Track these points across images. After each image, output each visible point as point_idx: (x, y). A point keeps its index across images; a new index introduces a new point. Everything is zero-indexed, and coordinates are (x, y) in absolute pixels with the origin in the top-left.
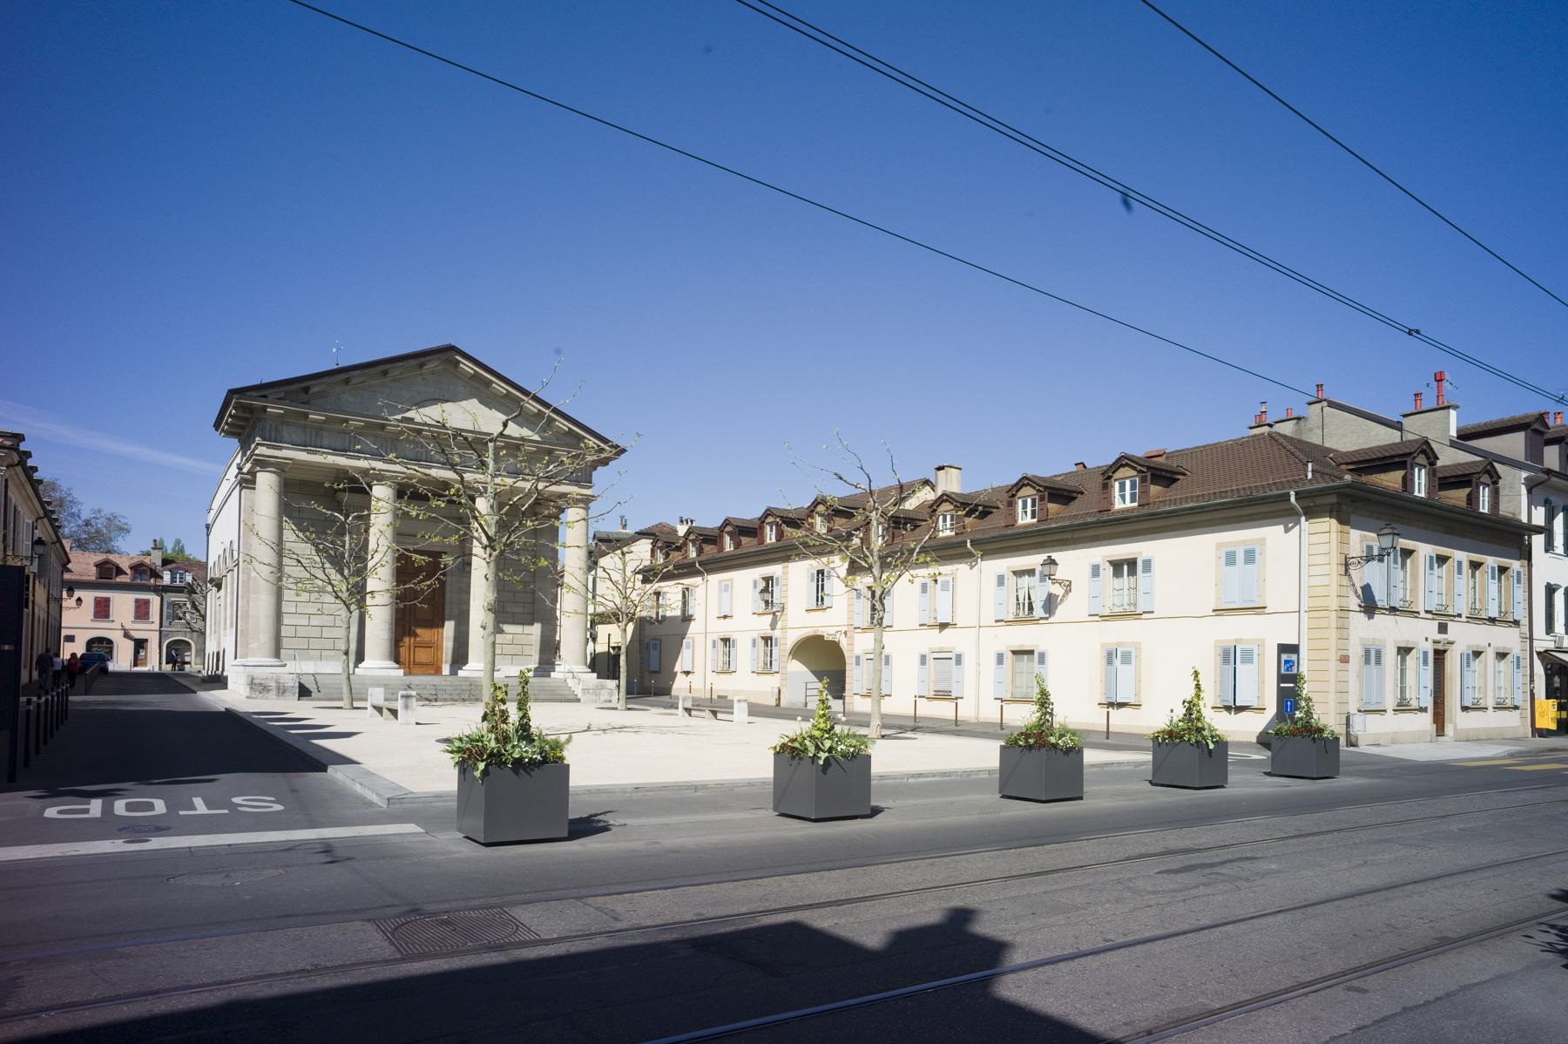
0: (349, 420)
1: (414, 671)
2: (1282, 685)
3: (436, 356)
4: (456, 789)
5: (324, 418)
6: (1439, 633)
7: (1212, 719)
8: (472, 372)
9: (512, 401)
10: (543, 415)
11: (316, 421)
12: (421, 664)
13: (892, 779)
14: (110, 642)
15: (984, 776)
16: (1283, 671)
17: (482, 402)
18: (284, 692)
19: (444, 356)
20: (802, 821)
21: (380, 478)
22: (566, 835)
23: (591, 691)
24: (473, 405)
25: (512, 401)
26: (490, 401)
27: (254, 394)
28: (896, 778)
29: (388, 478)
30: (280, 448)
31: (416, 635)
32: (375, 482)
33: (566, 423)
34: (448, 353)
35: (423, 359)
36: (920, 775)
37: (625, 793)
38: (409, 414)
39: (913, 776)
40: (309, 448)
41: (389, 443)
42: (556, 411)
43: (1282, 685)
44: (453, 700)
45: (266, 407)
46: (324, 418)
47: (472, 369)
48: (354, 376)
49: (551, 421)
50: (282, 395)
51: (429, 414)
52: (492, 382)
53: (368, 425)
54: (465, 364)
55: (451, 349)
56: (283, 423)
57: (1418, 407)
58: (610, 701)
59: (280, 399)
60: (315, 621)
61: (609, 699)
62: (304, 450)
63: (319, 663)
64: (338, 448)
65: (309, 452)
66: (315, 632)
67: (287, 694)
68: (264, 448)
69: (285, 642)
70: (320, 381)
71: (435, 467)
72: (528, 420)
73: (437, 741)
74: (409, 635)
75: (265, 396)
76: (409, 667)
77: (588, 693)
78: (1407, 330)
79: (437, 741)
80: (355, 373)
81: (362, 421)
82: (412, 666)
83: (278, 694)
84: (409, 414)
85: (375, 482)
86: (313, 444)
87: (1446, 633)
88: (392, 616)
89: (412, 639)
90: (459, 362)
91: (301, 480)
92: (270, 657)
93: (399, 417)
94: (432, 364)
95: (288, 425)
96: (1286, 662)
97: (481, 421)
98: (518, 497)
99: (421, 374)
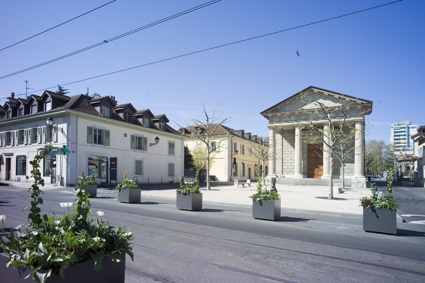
0: (285, 113)
2: (116, 169)
3: (307, 90)
4: (176, 197)
5: (361, 107)
7: (268, 187)
11: (279, 115)
13: (213, 203)
15: (250, 207)
17: (323, 99)
18: (269, 181)
19: (309, 90)
20: (106, 199)
21: (357, 122)
22: (128, 202)
23: (355, 183)
25: (331, 96)
27: (265, 112)
28: (214, 203)
30: (273, 124)
31: (319, 168)
32: (356, 123)
33: (349, 98)
36: (223, 203)
37: (149, 197)
38: (303, 108)
39: (221, 203)
40: (279, 122)
41: (298, 117)
42: (345, 96)
43: (116, 169)
45: (276, 114)
46: (361, 107)
47: (317, 91)
48: (286, 102)
49: (344, 99)
50: (271, 111)
52: (323, 93)
53: (291, 114)
54: (315, 90)
55: (311, 87)
56: (273, 118)
58: (363, 187)
61: (362, 186)
62: (278, 123)
64: (276, 122)
65: (279, 123)
67: (269, 182)
68: (270, 124)
70: (279, 105)
71: (320, 120)
73: (315, 197)
74: (317, 168)
75: (268, 112)
76: (317, 176)
77: (354, 184)
78: (108, 41)
79: (315, 197)
80: (286, 101)
81: (280, 114)
82: (318, 176)
83: (267, 182)
84: (303, 108)
85: (356, 123)
86: (281, 121)
87: (109, 146)
89: (318, 169)
91: (288, 130)
92: (362, 175)
93: (300, 109)
95: (274, 118)
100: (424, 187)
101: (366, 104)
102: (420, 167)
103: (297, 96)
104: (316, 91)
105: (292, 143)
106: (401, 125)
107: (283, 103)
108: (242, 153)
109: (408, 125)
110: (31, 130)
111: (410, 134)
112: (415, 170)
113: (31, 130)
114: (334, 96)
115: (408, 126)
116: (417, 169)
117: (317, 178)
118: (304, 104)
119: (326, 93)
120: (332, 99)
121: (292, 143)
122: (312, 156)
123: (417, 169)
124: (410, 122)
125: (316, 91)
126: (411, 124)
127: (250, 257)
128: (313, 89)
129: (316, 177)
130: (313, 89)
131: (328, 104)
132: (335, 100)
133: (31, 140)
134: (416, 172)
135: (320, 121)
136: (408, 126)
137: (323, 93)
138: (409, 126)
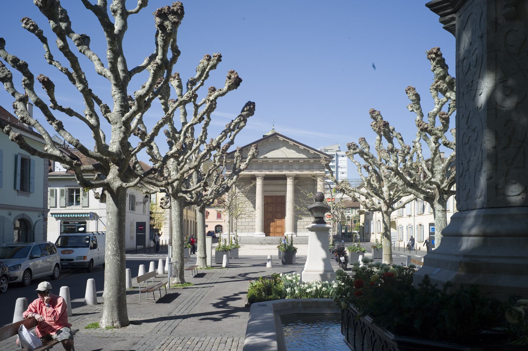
1: (276, 235)
6: (137, 223)
8: (282, 140)
9: (295, 145)
10: (306, 150)
12: (278, 233)
14: (221, 226)
16: (431, 231)
17: (287, 148)
19: (274, 136)
24: (284, 149)
26: (289, 147)
29: (259, 176)
33: (313, 151)
34: (275, 135)
35: (268, 139)
38: (265, 156)
44: (264, 244)
51: (270, 155)
57: (346, 167)
59: (230, 158)
60: (247, 220)
63: (248, 233)
66: (247, 224)
69: (298, 227)
72: (302, 151)
74: (273, 222)
84: (265, 156)
88: (262, 218)
90: (278, 137)
92: (260, 232)
94: (271, 140)
96: (432, 229)
97: (287, 154)
98: (21, 234)
99: (269, 143)
100: (370, 242)
101: (329, 159)
102: (367, 221)
103: (261, 142)
104: (281, 138)
105: (251, 195)
106: (329, 150)
107: (245, 148)
108: (18, 187)
109: (337, 152)
110: (66, 190)
111: (339, 166)
112: (361, 224)
113: (66, 190)
114: (299, 146)
115: (336, 153)
116: (363, 224)
117: (275, 236)
118: (267, 152)
119: (291, 143)
120: (297, 149)
121: (251, 195)
122: (269, 211)
123: (363, 224)
124: (339, 147)
125: (281, 138)
126: (340, 151)
127: (216, 332)
128: (278, 136)
129: (274, 235)
130: (278, 136)
131: (292, 154)
132: (299, 151)
133: (66, 202)
134: (362, 226)
135: (284, 173)
136: (336, 153)
137: (288, 142)
138: (339, 153)
